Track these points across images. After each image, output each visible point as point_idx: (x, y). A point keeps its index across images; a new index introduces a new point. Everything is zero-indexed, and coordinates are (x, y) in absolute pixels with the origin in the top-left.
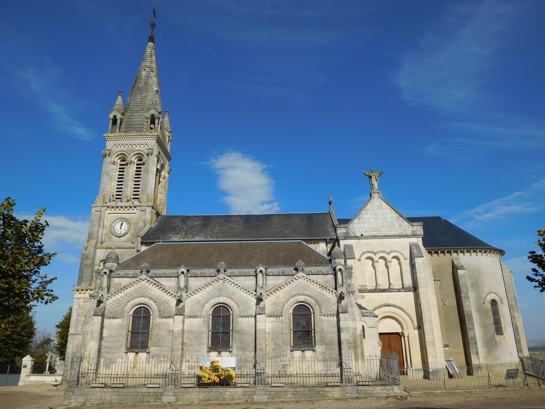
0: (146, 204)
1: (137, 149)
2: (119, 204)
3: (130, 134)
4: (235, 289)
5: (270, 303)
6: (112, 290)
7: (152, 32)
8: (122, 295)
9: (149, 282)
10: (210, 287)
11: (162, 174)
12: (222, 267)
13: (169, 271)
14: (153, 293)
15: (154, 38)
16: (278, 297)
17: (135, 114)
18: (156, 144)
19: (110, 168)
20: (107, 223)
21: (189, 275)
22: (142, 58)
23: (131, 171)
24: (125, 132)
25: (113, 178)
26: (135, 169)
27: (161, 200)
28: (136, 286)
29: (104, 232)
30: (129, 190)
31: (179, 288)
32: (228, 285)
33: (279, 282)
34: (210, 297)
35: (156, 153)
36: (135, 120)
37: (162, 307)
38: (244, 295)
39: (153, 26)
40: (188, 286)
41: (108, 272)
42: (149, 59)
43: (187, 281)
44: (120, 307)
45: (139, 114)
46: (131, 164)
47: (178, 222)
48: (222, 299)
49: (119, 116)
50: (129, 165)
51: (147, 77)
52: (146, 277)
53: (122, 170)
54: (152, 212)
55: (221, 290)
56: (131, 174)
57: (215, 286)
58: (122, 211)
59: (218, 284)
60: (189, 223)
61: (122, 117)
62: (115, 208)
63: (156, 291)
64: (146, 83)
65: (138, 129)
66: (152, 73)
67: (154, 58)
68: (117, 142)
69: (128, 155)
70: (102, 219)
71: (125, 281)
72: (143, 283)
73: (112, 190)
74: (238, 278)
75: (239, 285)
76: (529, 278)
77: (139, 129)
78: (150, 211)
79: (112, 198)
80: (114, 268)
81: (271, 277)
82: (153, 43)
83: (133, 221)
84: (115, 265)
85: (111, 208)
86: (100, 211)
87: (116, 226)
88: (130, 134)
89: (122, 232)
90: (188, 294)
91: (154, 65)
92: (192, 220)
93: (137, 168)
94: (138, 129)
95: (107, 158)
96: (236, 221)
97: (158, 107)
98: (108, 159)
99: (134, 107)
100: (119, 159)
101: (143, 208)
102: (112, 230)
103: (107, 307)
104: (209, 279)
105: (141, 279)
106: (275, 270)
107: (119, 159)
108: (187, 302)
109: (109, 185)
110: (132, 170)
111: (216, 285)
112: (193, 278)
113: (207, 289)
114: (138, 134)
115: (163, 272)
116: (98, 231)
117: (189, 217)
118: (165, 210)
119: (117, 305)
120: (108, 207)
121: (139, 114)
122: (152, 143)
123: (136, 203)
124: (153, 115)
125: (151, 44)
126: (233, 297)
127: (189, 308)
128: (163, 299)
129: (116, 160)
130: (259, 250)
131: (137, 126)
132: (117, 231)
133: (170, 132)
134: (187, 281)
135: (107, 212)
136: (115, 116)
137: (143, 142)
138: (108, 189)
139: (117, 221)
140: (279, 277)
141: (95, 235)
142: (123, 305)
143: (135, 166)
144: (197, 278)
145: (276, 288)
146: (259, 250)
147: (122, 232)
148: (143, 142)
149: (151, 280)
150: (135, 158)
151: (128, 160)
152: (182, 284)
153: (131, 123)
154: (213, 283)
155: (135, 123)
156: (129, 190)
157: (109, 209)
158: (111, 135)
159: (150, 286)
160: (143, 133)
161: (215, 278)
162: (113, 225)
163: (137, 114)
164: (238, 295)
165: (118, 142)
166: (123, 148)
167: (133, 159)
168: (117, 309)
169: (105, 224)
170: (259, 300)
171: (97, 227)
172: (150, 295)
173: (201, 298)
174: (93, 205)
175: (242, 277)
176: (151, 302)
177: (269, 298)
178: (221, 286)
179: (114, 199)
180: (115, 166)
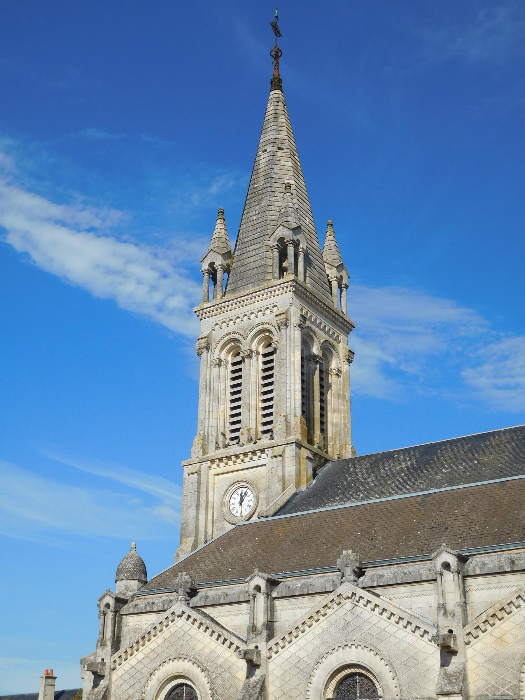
0: (283, 441)
1: (258, 321)
2: (235, 449)
3: (242, 293)
4: (384, 623)
5: (481, 660)
6: (125, 644)
7: (277, 68)
8: (139, 656)
9: (418, 633)
10: (324, 623)
11: (333, 365)
12: (347, 565)
13: (234, 590)
14: (200, 646)
15: (280, 81)
16: (500, 639)
17: (249, 249)
18: (297, 302)
19: (215, 379)
20: (214, 497)
21: (274, 595)
22: (260, 128)
23: (253, 371)
24: (234, 290)
25: (222, 396)
26: (261, 366)
27: (336, 425)
28: (166, 633)
29: (210, 518)
30: (252, 417)
31: (253, 629)
32: (365, 612)
33: (506, 592)
34: (323, 650)
35: (295, 319)
36: (250, 260)
37: (219, 681)
38: (408, 637)
39: (277, 55)
40: (276, 624)
41: (112, 602)
42: (272, 125)
43: (271, 610)
44: (137, 686)
45: (258, 246)
46: (250, 356)
47: (361, 471)
48: (353, 655)
49: (219, 261)
50: (247, 360)
51: (270, 163)
52: (184, 608)
53: (237, 374)
54: (298, 457)
55: (350, 629)
56: (253, 379)
57: (333, 618)
58: (231, 466)
59: (342, 612)
60: (383, 471)
61: (228, 261)
62: (225, 460)
63: (205, 643)
64: (268, 178)
65: (257, 278)
66: (279, 153)
67: (283, 120)
68: (219, 318)
69: (242, 340)
70: (203, 489)
71: (147, 621)
72: (181, 622)
73: (221, 423)
74: (392, 590)
75: (391, 609)
76: (354, 327)
77: (258, 278)
78: (293, 453)
79: (221, 438)
80: (131, 593)
81: (480, 580)
82: (280, 89)
83: (263, 483)
84: (135, 585)
85: (217, 462)
86: (198, 473)
87: (232, 501)
88: (242, 293)
89: (244, 513)
90: (272, 643)
91: (284, 135)
92: (396, 460)
93: (265, 363)
94: (257, 278)
95: (204, 354)
96: (498, 446)
97: (289, 219)
98: (207, 357)
99: (248, 234)
100: (228, 352)
101: (278, 450)
102: (226, 509)
103: (113, 688)
104: (322, 600)
105: (173, 613)
106: (492, 560)
107: (228, 352)
108: (272, 665)
109: (214, 414)
110: (254, 368)
111: (338, 614)
112: (285, 601)
113: (317, 628)
114: (257, 289)
115: (220, 592)
116: (197, 518)
117: (389, 456)
118: (349, 449)
119: (132, 682)
120: (213, 461)
121: (258, 246)
122: (285, 299)
123: (265, 441)
124: (281, 240)
125: (275, 94)
126: (381, 646)
127: (278, 683)
128: (220, 661)
129: (223, 356)
130: (467, 506)
131: (253, 272)
132: (234, 512)
133: (340, 267)
134: (271, 610)
135: (212, 472)
136: (212, 264)
137: (266, 302)
138: (213, 422)
139: (232, 489)
140: (502, 578)
141: (191, 528)
142: (143, 681)
143: (261, 359)
144: (294, 600)
145: (491, 612)
146: (467, 506)
147: (244, 513)
148: (266, 302)
149: (194, 615)
150: (259, 343)
151: (244, 347)
152: (261, 619)
153: (242, 269)
154: (329, 612)
155: (250, 266)
156: (252, 417)
157: (214, 466)
158: (206, 305)
159: (193, 629)
160: (266, 284)
161: (331, 596)
162: (227, 499)
163: (253, 247)
164: (392, 639)
165: (222, 317)
166: (232, 328)
167: (254, 347)
168: (131, 691)
169: (210, 499)
170: (448, 652)
171: (194, 508)
172: (192, 654)
173: (302, 654)
174: (184, 463)
175: (403, 588)
176: (195, 671)
177: (477, 645)
178: (349, 618)
179: (228, 441)
180: (222, 369)
